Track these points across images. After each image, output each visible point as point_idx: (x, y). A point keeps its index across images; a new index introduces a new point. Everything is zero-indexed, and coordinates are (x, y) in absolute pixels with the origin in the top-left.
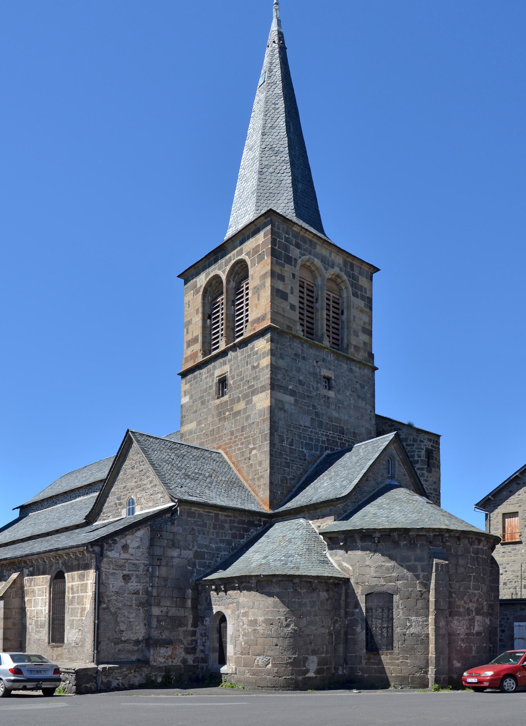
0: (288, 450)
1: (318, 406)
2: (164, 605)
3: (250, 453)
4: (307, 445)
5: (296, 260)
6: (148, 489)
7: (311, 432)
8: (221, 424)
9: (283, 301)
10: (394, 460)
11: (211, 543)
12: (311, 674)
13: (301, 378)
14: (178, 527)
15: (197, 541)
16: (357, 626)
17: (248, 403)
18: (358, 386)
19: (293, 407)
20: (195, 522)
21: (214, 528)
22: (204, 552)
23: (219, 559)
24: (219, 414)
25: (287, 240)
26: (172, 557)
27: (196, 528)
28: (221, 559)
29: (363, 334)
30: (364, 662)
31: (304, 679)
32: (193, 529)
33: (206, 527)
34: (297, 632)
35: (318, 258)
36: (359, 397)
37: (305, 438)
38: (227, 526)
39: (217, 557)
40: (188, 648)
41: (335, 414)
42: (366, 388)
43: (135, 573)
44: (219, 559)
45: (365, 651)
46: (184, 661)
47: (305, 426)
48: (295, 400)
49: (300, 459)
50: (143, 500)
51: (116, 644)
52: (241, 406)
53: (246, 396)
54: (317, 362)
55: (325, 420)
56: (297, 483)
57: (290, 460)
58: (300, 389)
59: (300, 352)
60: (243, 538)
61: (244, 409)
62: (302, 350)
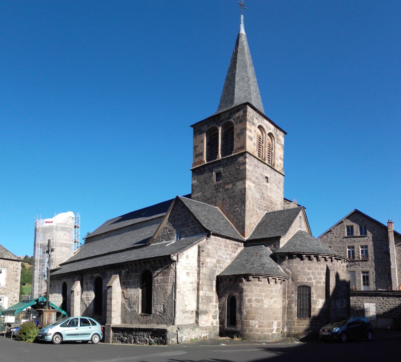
0: (252, 209)
1: (263, 190)
2: (204, 290)
3: (235, 209)
4: (259, 207)
5: (256, 124)
6: (190, 225)
7: (260, 201)
8: (217, 194)
9: (251, 141)
10: (301, 219)
11: (223, 255)
12: (274, 332)
13: (257, 176)
14: (210, 246)
15: (217, 254)
16: (293, 304)
17: (233, 185)
18: (277, 182)
19: (254, 189)
20: (217, 243)
21: (225, 247)
22: (220, 260)
23: (226, 264)
24: (216, 189)
25: (253, 115)
26: (208, 262)
27: (217, 247)
28: (227, 264)
29: (280, 160)
30: (296, 324)
31: (272, 334)
32: (216, 247)
33: (221, 246)
34: (270, 307)
35: (265, 125)
36: (278, 187)
37: (258, 204)
38: (230, 246)
39: (226, 263)
40: (214, 316)
41: (269, 194)
42: (281, 183)
43: (191, 271)
44: (226, 264)
45: (297, 318)
46: (212, 324)
47: (258, 199)
48: (255, 186)
49: (256, 214)
50: (186, 232)
51: (184, 313)
52: (230, 186)
53: (232, 182)
54: (263, 170)
55: (265, 196)
56: (255, 226)
57: (253, 214)
58: (257, 181)
59: (257, 164)
60: (235, 253)
61: (231, 188)
62: (258, 163)
